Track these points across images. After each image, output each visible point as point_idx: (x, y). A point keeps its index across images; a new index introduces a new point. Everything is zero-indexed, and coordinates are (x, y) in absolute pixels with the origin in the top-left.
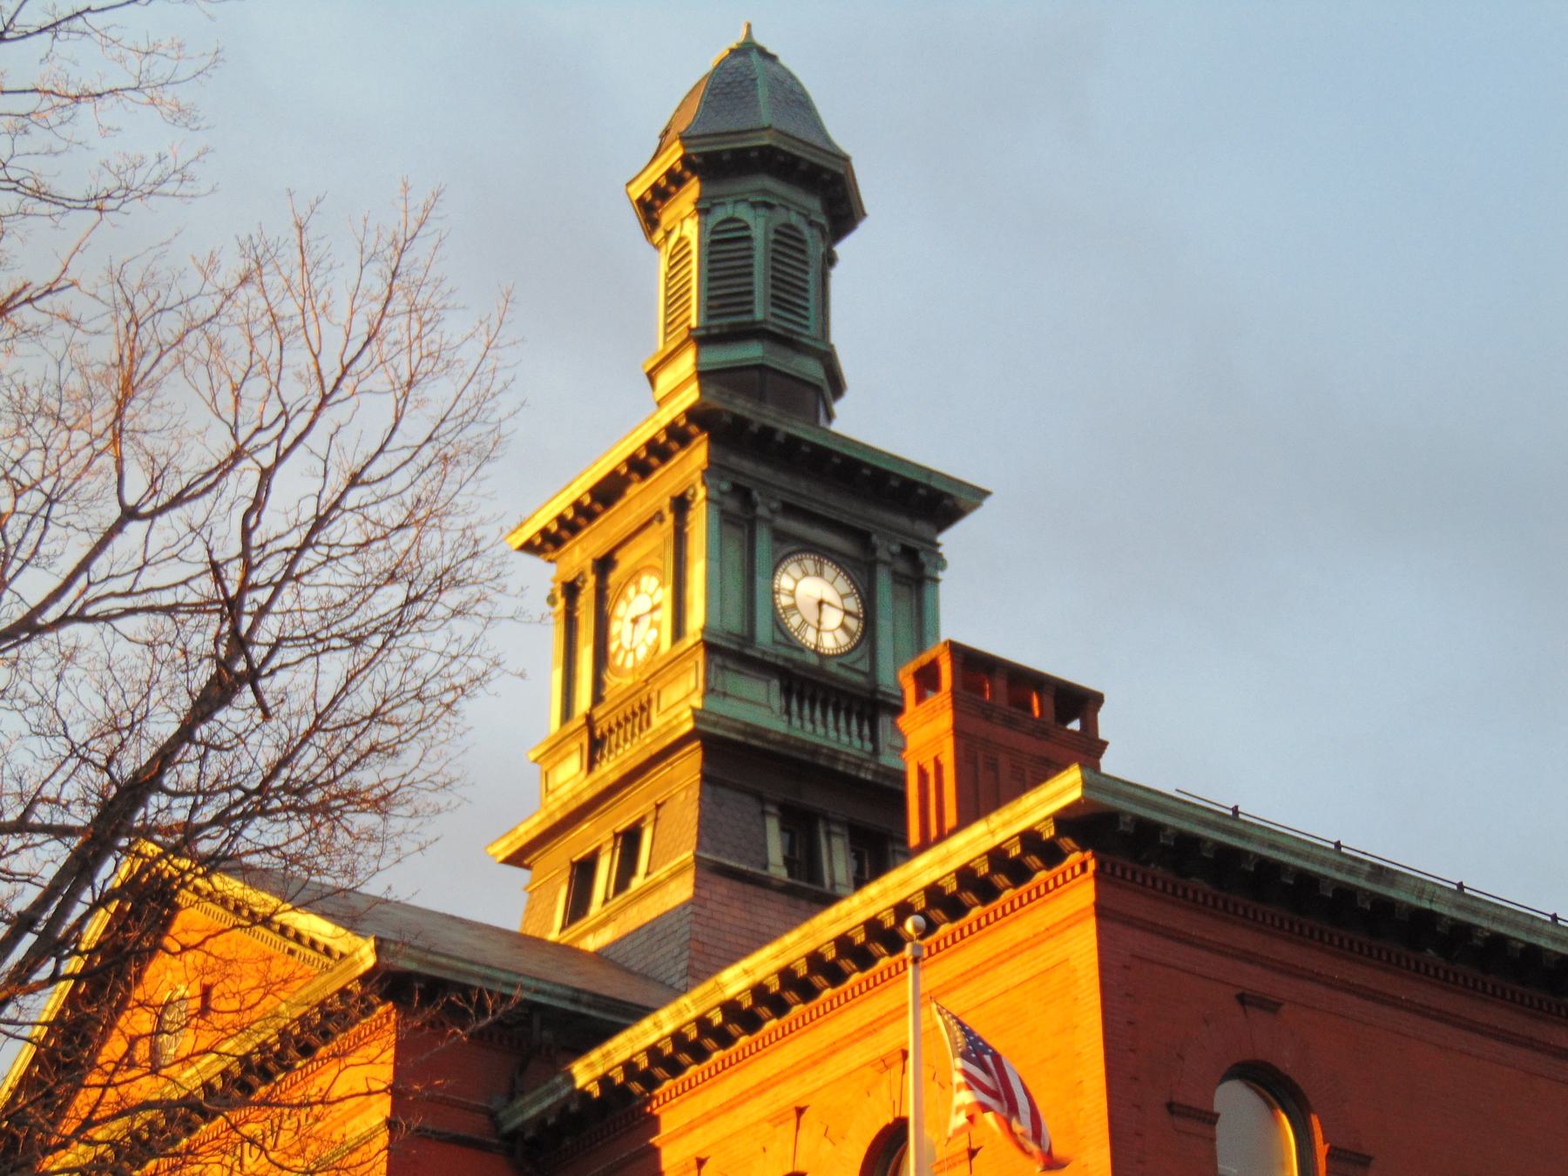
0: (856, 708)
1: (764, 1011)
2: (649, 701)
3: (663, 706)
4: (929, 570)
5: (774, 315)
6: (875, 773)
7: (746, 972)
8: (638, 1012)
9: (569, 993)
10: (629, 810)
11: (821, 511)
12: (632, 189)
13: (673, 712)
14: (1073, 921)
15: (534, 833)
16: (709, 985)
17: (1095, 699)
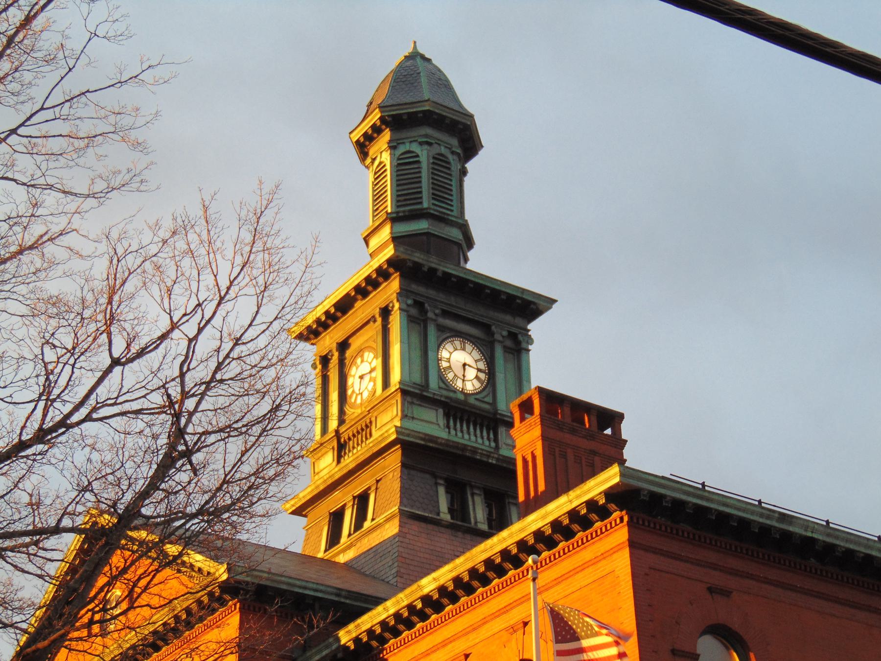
0: (486, 423)
1: (445, 601)
2: (371, 422)
3: (378, 426)
4: (524, 345)
5: (433, 204)
6: (498, 459)
7: (434, 579)
8: (378, 601)
9: (335, 591)
10: (361, 484)
11: (463, 313)
12: (352, 136)
13: (385, 429)
15: (308, 497)
16: (414, 587)
17: (620, 417)
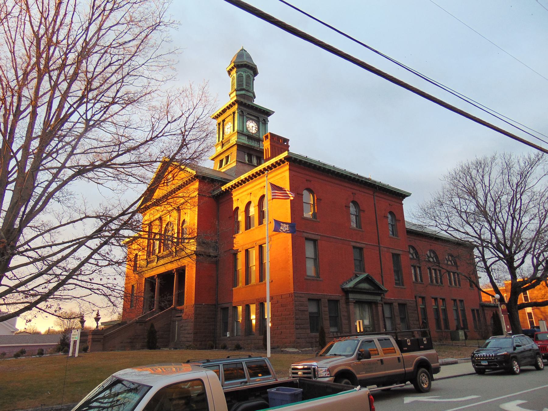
8: (231, 181)
14: (286, 170)
